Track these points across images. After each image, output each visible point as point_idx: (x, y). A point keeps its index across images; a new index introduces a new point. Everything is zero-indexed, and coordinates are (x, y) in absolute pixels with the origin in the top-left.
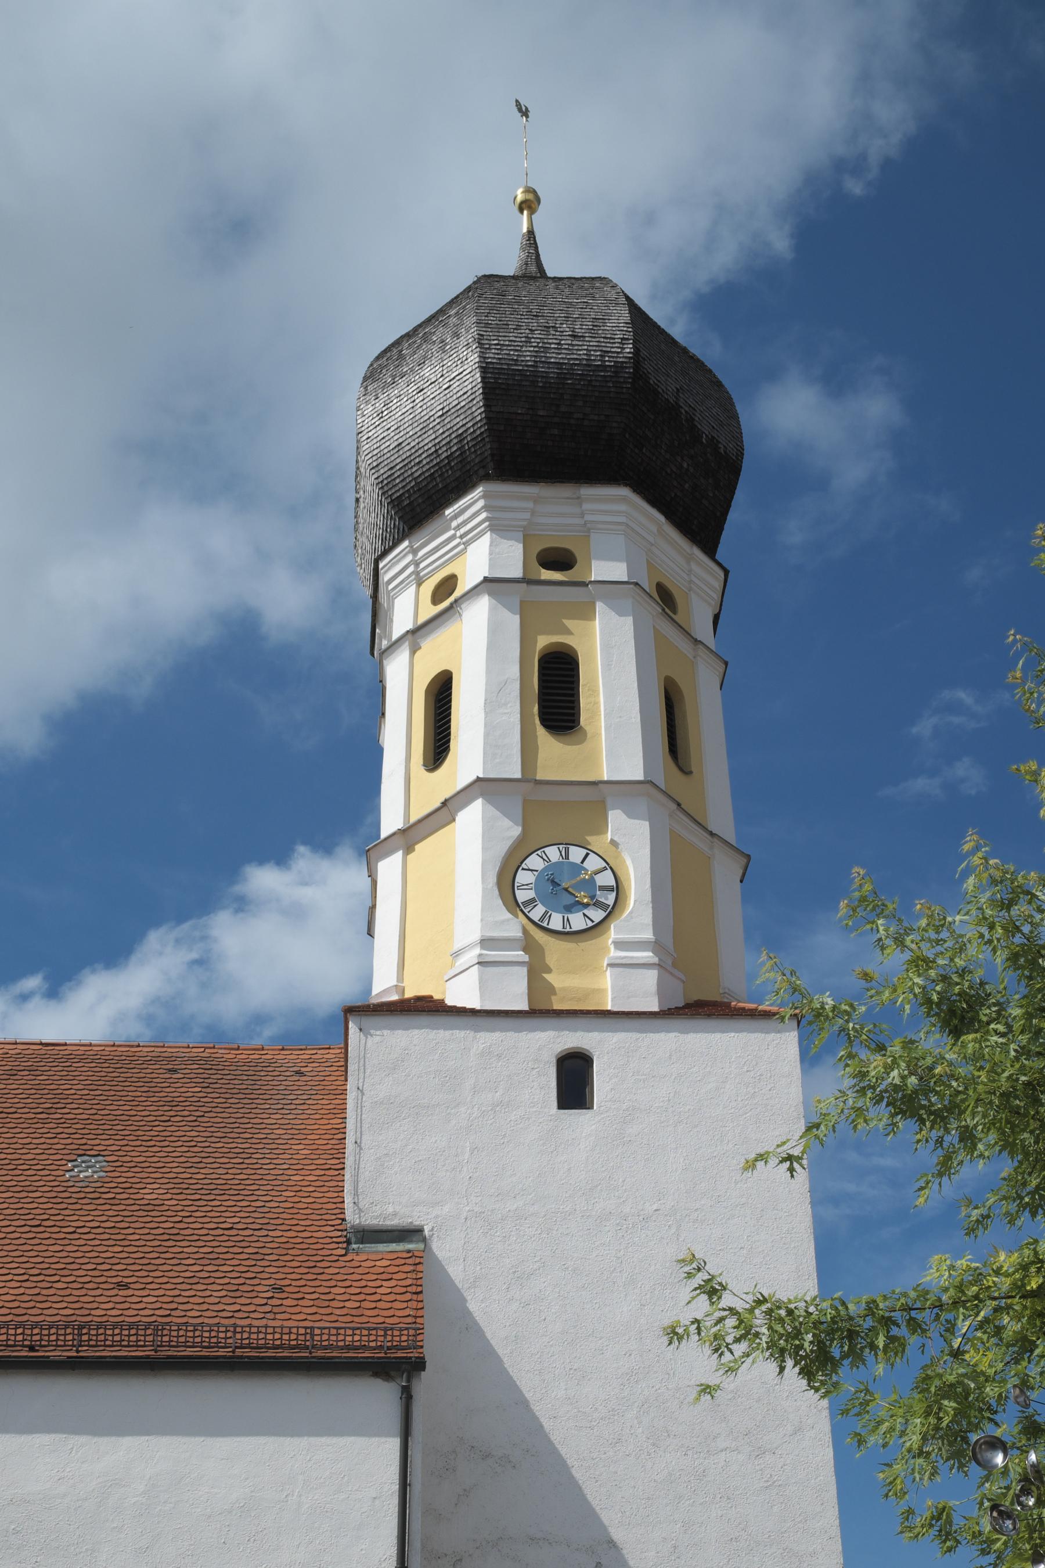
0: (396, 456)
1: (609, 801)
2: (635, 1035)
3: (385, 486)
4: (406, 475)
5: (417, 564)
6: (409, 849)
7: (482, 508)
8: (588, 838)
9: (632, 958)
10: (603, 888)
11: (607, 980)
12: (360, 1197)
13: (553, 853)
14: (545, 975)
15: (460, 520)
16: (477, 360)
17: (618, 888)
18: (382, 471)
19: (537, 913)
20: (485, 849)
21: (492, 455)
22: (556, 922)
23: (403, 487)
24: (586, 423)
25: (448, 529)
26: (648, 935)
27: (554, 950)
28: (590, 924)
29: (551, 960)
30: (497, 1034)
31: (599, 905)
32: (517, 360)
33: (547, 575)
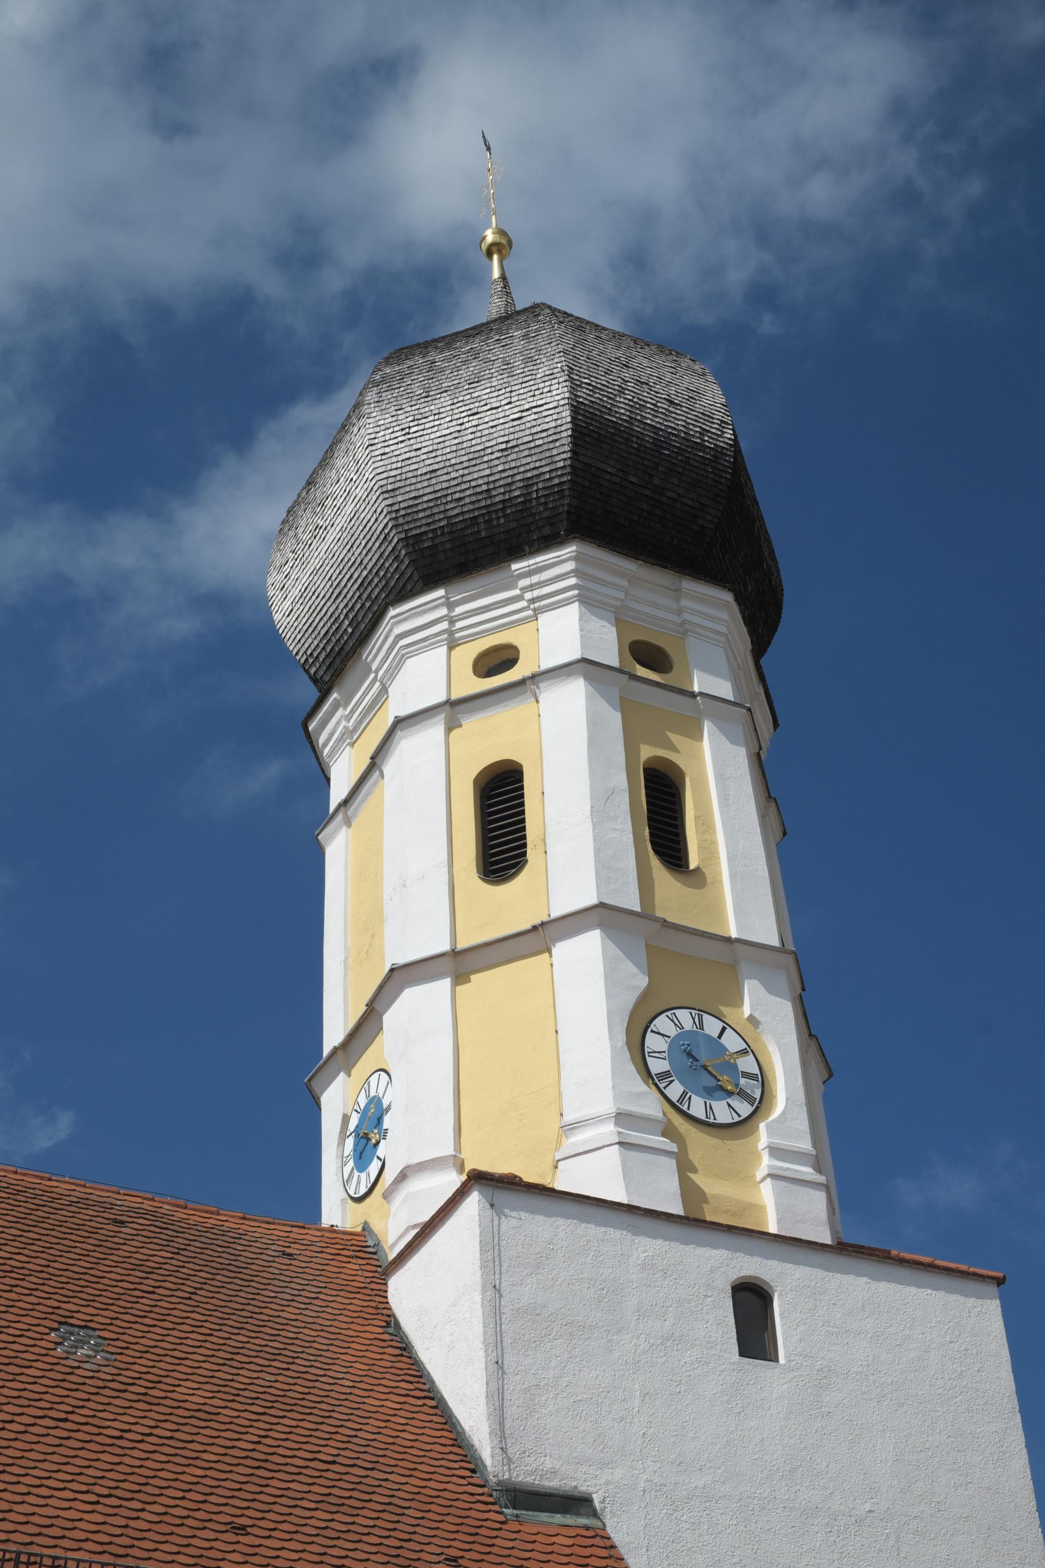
0: (426, 484)
1: (744, 967)
2: (820, 1273)
3: (400, 517)
4: (435, 510)
5: (452, 622)
6: (460, 978)
7: (572, 571)
8: (722, 1008)
9: (800, 1172)
10: (745, 1075)
11: (767, 1194)
12: (508, 1441)
13: (685, 1017)
14: (690, 1175)
15: (535, 579)
16: (567, 395)
17: (763, 1079)
18: (400, 498)
19: (675, 1091)
20: (609, 996)
21: (569, 513)
22: (697, 1107)
23: (428, 524)
24: (678, 505)
25: (512, 586)
26: (806, 1145)
27: (698, 1141)
28: (737, 1119)
29: (695, 1156)
30: (659, 1242)
31: (743, 1094)
32: (610, 409)
33: (642, 672)
